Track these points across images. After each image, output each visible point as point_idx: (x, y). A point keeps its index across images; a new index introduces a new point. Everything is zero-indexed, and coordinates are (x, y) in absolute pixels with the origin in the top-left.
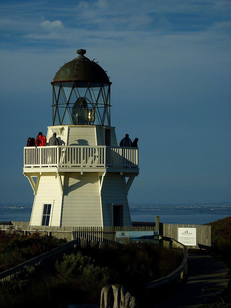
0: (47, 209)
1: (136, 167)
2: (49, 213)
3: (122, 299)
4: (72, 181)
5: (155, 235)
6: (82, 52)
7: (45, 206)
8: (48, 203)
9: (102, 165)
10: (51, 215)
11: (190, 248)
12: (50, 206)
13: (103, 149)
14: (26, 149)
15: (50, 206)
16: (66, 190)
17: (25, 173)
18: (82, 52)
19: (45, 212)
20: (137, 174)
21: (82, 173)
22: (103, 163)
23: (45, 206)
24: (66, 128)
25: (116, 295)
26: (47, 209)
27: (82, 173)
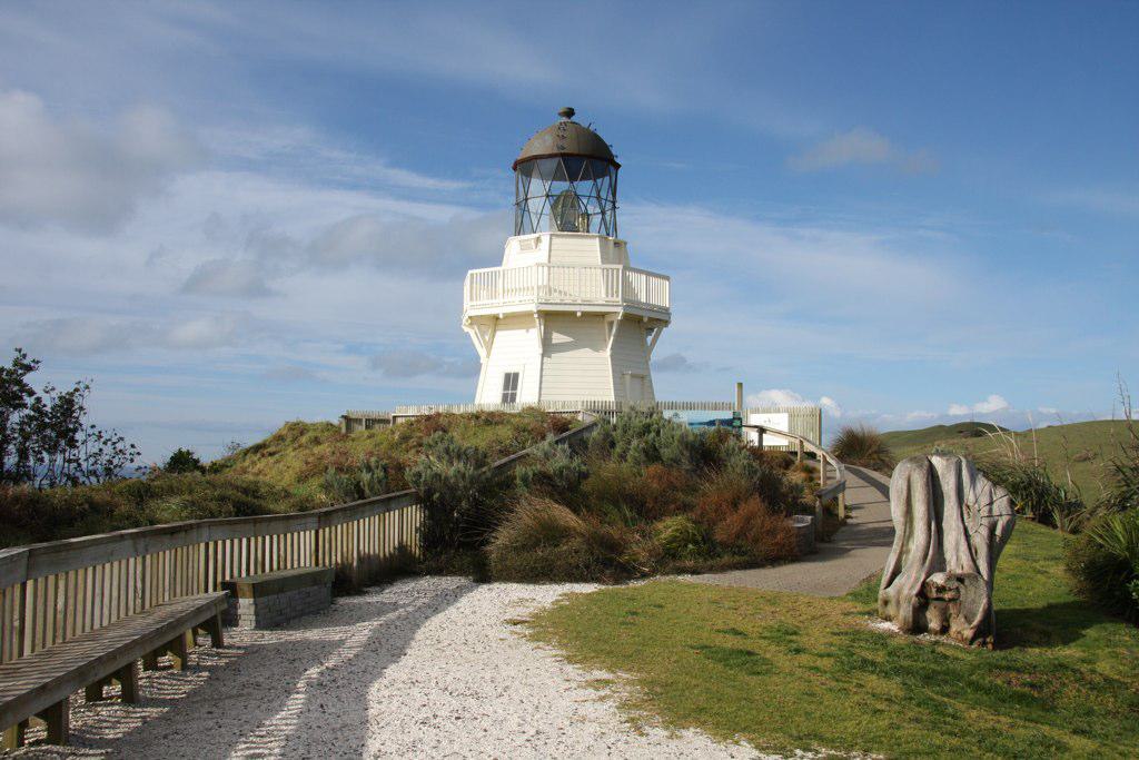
0: (511, 381)
1: (666, 311)
2: (515, 387)
3: (969, 496)
4: (557, 338)
5: (734, 418)
6: (570, 113)
7: (508, 376)
8: (512, 370)
9: (615, 299)
10: (518, 392)
11: (387, 514)
12: (516, 376)
13: (618, 270)
14: (472, 275)
15: (516, 376)
16: (548, 348)
17: (474, 320)
18: (570, 113)
19: (506, 387)
20: (666, 323)
21: (579, 314)
22: (617, 296)
23: (508, 376)
24: (545, 239)
25: (948, 486)
26: (511, 381)
27: (579, 314)
